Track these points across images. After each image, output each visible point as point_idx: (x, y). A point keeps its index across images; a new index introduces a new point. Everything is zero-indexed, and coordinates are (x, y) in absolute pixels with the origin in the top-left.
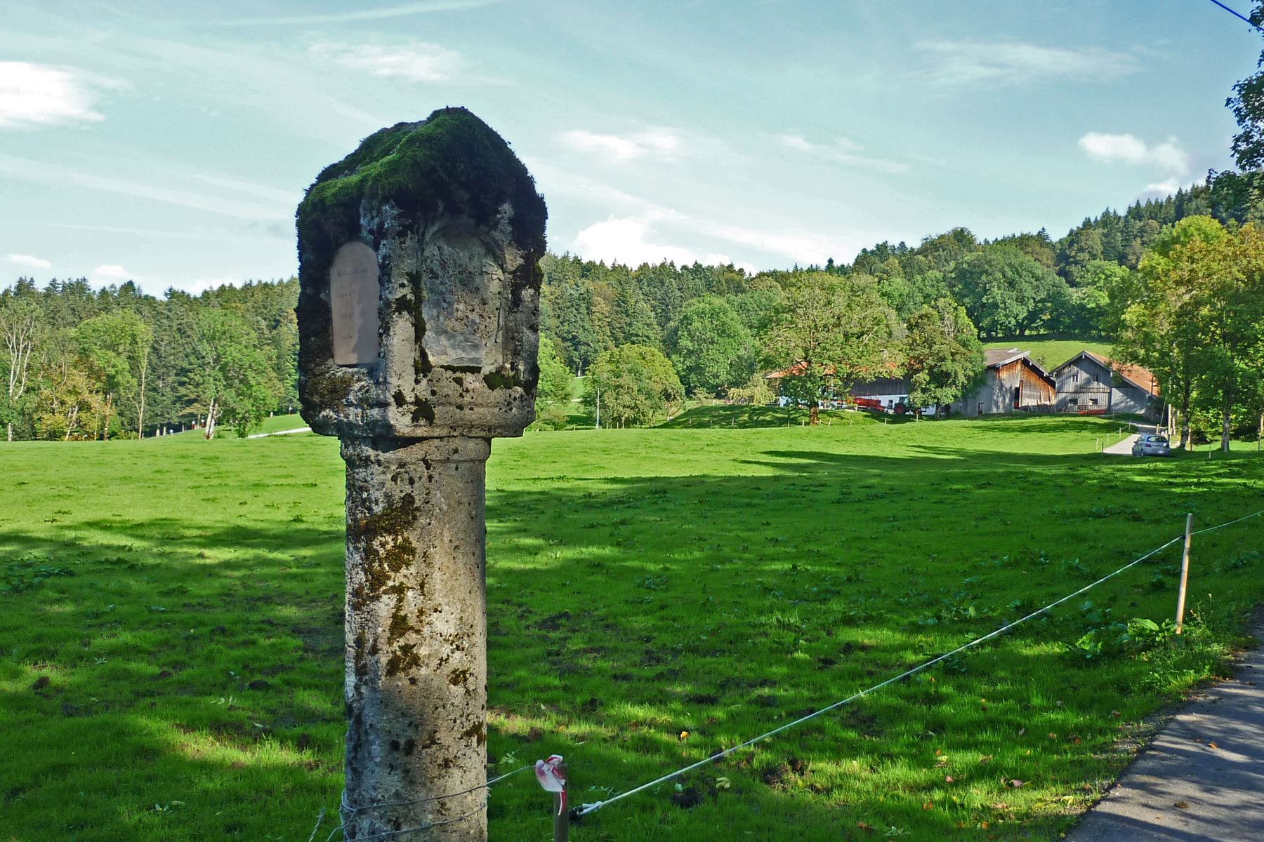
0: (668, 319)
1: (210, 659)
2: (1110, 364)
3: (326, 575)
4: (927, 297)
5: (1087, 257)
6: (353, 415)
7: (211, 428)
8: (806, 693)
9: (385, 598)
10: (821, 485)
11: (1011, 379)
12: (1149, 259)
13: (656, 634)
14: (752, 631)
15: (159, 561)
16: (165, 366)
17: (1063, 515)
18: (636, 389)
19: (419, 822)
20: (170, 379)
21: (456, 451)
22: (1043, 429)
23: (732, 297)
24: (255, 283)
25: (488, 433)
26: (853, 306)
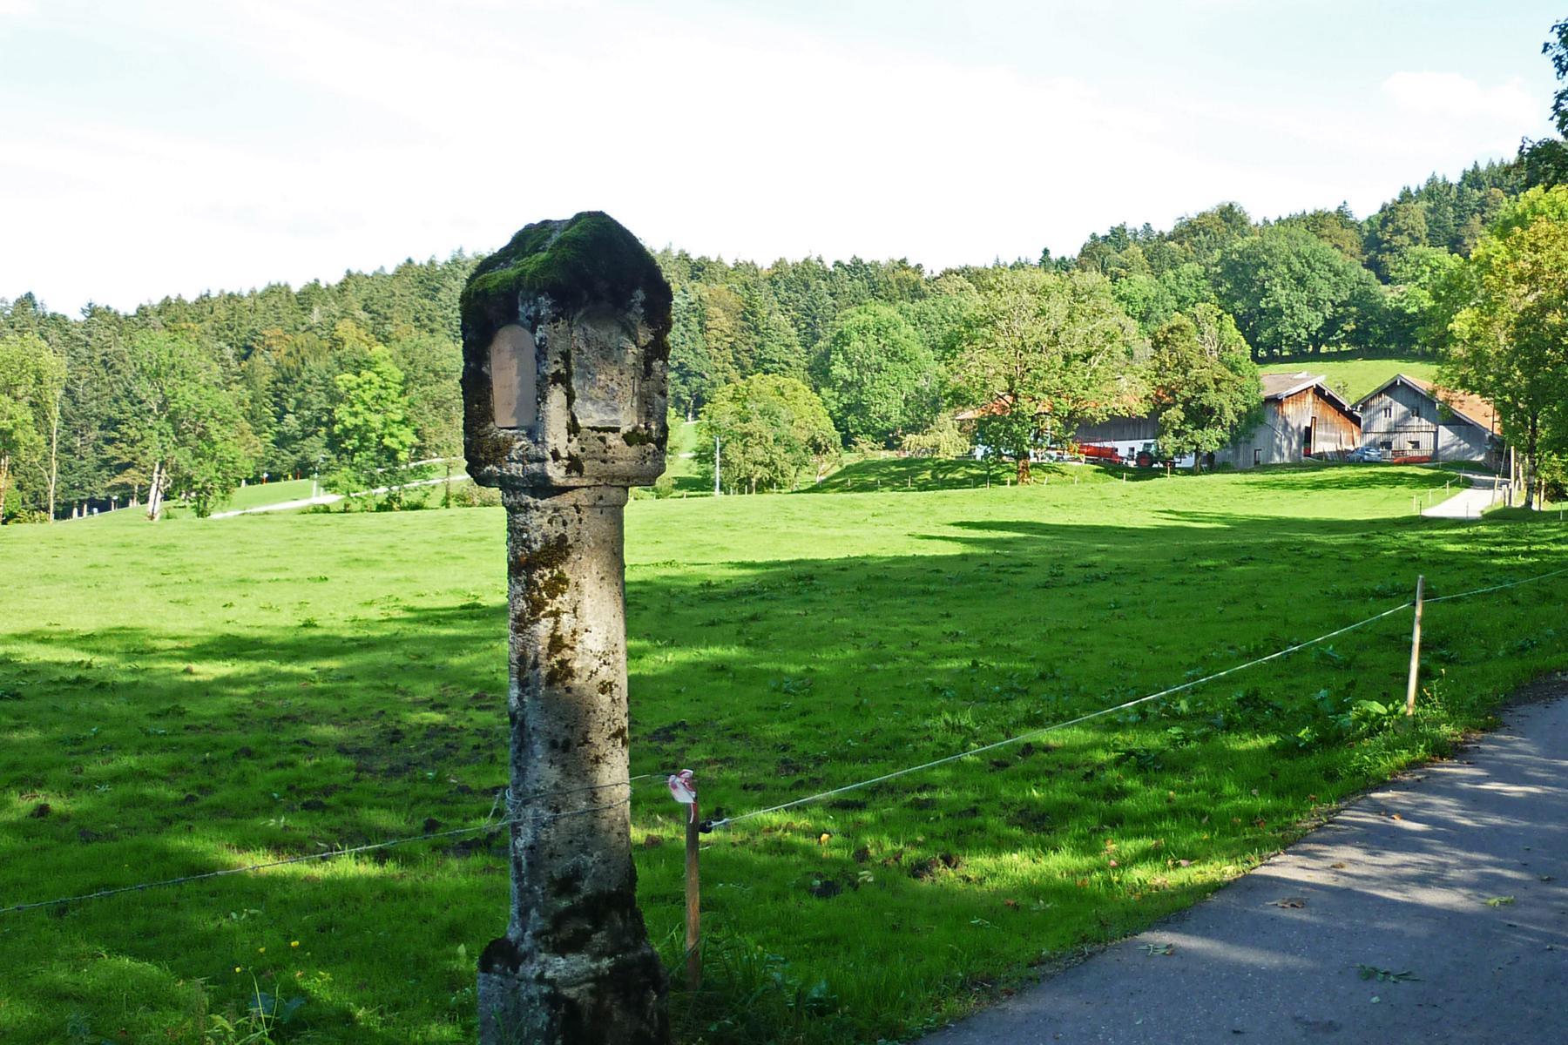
0: (816, 338)
1: (242, 781)
2: (1434, 392)
3: (364, 689)
4: (1182, 300)
5: (1407, 240)
6: (515, 469)
7: (156, 503)
8: (970, 795)
9: (544, 621)
10: (1024, 565)
11: (1300, 414)
12: (1485, 245)
13: (795, 742)
14: (914, 735)
15: (134, 679)
16: (83, 416)
17: (1337, 595)
18: (771, 438)
19: (575, 808)
20: (92, 435)
21: (601, 498)
22: (1342, 484)
23: (906, 305)
24: (214, 294)
25: (626, 482)
26: (1076, 316)
